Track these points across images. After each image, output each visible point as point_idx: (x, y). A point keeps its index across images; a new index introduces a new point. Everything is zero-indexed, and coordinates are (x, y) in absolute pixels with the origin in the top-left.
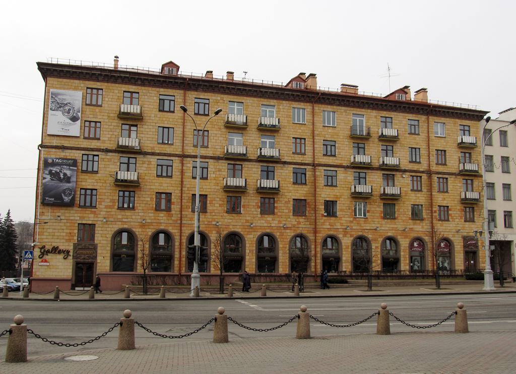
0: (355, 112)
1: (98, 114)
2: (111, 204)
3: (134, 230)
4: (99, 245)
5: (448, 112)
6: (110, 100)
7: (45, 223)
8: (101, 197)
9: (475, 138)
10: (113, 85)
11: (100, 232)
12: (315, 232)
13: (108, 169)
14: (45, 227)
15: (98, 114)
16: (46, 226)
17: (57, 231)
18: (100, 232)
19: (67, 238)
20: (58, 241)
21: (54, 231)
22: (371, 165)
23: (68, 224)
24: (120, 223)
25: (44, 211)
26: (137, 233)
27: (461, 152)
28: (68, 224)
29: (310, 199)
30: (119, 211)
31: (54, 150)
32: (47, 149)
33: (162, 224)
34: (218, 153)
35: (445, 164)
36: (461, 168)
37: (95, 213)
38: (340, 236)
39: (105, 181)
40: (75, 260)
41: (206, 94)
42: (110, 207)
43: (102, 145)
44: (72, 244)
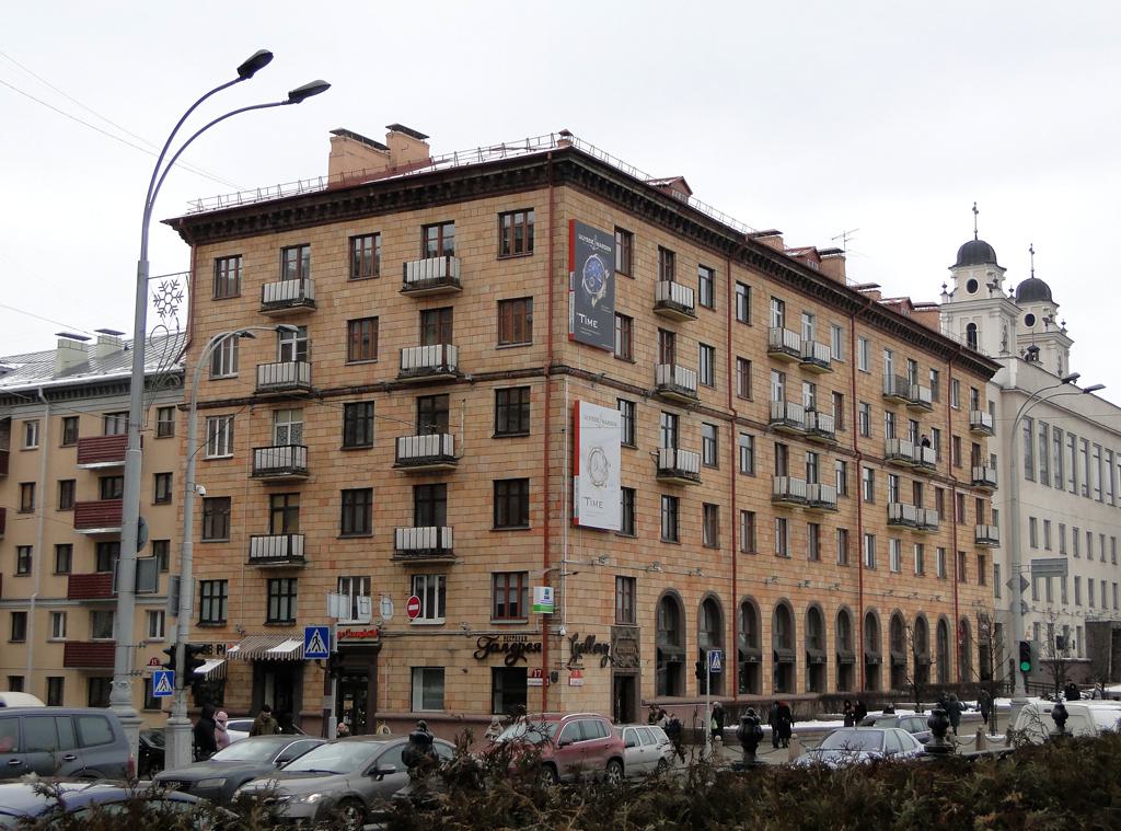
7: (575, 573)
10: (646, 226)
43: (637, 377)
44: (609, 630)
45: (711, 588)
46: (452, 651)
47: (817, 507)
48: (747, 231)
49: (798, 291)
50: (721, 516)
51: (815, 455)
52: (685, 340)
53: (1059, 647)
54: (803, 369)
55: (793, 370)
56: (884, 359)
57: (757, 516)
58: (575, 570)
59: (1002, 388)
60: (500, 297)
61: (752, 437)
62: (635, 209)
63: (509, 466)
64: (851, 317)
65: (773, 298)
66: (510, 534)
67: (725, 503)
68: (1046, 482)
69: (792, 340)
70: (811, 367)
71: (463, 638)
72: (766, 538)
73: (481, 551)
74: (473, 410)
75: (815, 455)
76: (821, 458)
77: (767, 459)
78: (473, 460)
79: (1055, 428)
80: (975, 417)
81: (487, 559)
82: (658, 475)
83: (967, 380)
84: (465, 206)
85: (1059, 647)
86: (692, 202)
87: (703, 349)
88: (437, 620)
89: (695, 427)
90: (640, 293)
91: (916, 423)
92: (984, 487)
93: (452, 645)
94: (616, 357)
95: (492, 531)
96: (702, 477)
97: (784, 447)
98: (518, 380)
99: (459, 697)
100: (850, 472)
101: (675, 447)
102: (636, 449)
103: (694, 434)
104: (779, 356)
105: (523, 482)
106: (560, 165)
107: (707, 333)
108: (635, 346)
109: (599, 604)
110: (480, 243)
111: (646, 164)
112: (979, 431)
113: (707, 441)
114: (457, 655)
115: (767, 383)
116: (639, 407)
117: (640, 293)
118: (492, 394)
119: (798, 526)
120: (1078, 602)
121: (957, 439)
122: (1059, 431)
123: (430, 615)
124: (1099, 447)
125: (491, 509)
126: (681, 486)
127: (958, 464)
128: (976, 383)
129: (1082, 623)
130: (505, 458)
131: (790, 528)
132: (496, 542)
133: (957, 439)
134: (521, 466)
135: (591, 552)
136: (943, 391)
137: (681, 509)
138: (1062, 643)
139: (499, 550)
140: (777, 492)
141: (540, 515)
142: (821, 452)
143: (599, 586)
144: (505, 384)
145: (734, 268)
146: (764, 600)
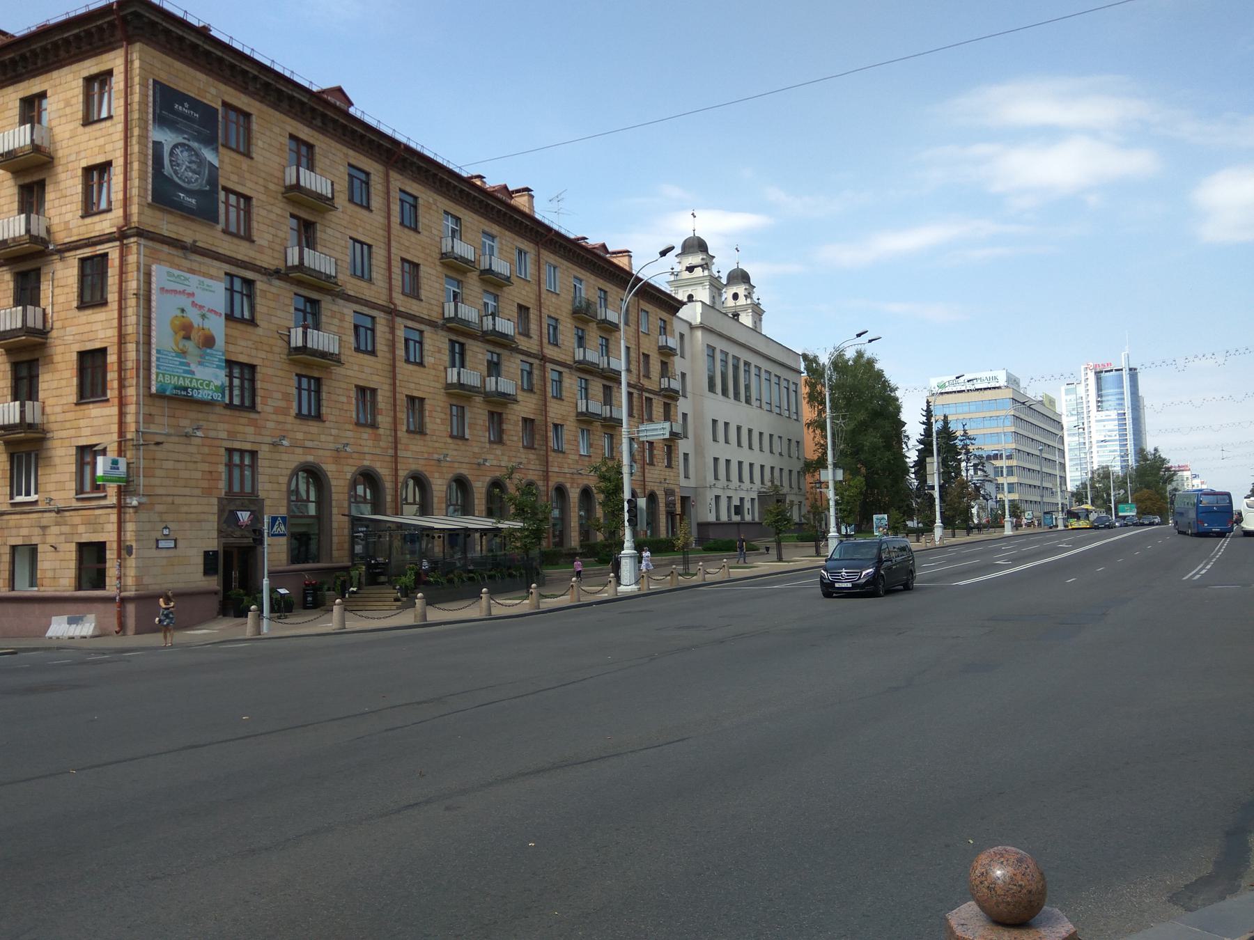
0: (487, 229)
1: (247, 175)
2: (283, 404)
3: (324, 466)
4: (267, 502)
5: (220, 60)
6: (266, 146)
7: (158, 444)
8: (266, 386)
9: (329, 183)
10: (271, 111)
11: (268, 471)
12: (546, 478)
13: (274, 320)
14: (159, 455)
15: (247, 175)
16: (160, 453)
17: (182, 465)
18: (268, 471)
19: (205, 484)
20: (187, 491)
21: (178, 466)
22: (336, 284)
23: (206, 450)
24: (299, 451)
25: (154, 411)
26: (329, 474)
27: (292, 216)
28: (206, 450)
29: (539, 419)
30: (298, 421)
31: (165, 248)
32: (150, 243)
33: (367, 457)
34: (435, 316)
35: (249, 238)
36: (450, 311)
37: (253, 423)
38: (568, 485)
39: (271, 346)
40: (223, 540)
41: (415, 185)
42: (283, 411)
43: (258, 256)
44: (215, 501)
45: (367, 463)
46: (44, 528)
47: (504, 399)
48: (572, 237)
49: (476, 211)
50: (380, 398)
51: (499, 355)
52: (329, 231)
53: (736, 513)
54: (483, 281)
55: (473, 280)
56: (565, 285)
57: (427, 401)
58: (159, 439)
59: (690, 324)
60: (84, 164)
61: (421, 332)
62: (251, 88)
63: (92, 336)
64: (537, 244)
65: (446, 213)
66: (91, 406)
67: (386, 387)
68: (748, 401)
69: (464, 249)
70: (493, 282)
71: (53, 514)
72: (438, 421)
73: (68, 425)
74: (61, 282)
75: (499, 355)
76: (503, 357)
77: (439, 352)
78: (61, 333)
79: (734, 357)
80: (662, 340)
81: (72, 432)
82: (289, 354)
83: (656, 314)
84: (55, 74)
85: (736, 513)
86: (352, 110)
87: (358, 246)
88: (33, 497)
89: (513, 365)
90: (263, 175)
91: (607, 340)
92: (671, 396)
93: (44, 522)
94: (226, 231)
95: (76, 404)
96: (519, 398)
97: (462, 345)
98: (99, 247)
99: (49, 574)
100: (536, 372)
101: (587, 399)
102: (256, 325)
103: (342, 320)
104: (455, 266)
105: (103, 351)
106: (129, 18)
107: (360, 230)
108: (255, 225)
109: (198, 475)
110: (68, 110)
111: (314, 77)
112: (666, 352)
113: (411, 343)
114: (48, 531)
115: (433, 282)
116: (260, 286)
117: (263, 175)
118: (76, 263)
119: (478, 414)
120: (752, 481)
121: (647, 356)
122: (747, 364)
123: (28, 494)
124: (770, 373)
125: (75, 381)
126: (504, 405)
127: (647, 376)
128: (664, 315)
129: (755, 496)
130: (87, 328)
131: (468, 415)
132: (80, 414)
133: (647, 356)
134: (101, 335)
135: (184, 422)
136: (632, 318)
137: (324, 389)
138: (739, 510)
139: (82, 423)
140: (449, 381)
141: (115, 384)
142: (505, 353)
143: (199, 458)
144: (87, 252)
145: (394, 175)
146: (436, 475)
